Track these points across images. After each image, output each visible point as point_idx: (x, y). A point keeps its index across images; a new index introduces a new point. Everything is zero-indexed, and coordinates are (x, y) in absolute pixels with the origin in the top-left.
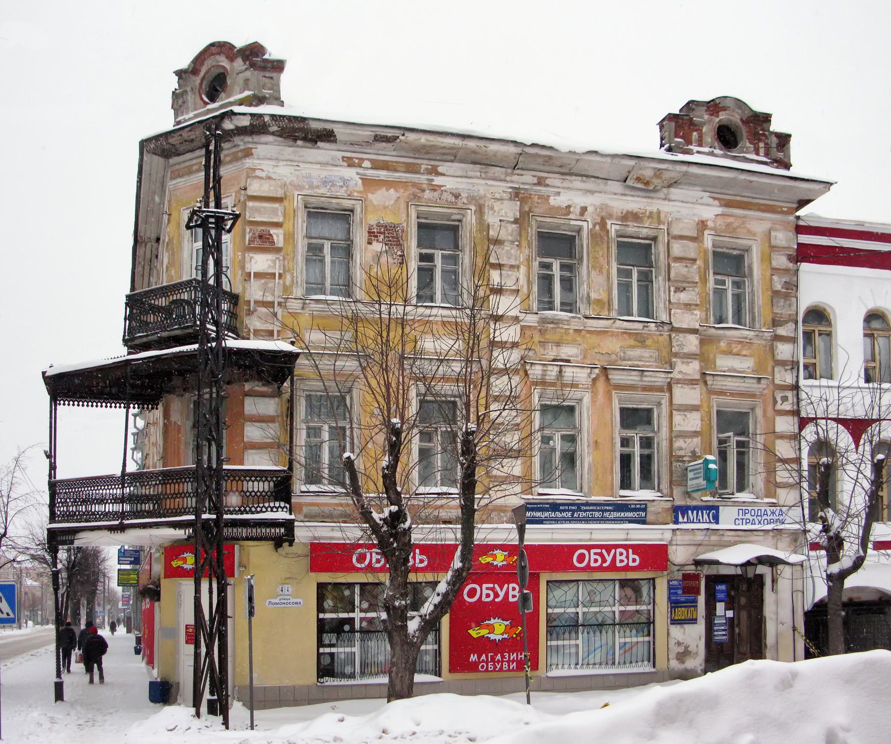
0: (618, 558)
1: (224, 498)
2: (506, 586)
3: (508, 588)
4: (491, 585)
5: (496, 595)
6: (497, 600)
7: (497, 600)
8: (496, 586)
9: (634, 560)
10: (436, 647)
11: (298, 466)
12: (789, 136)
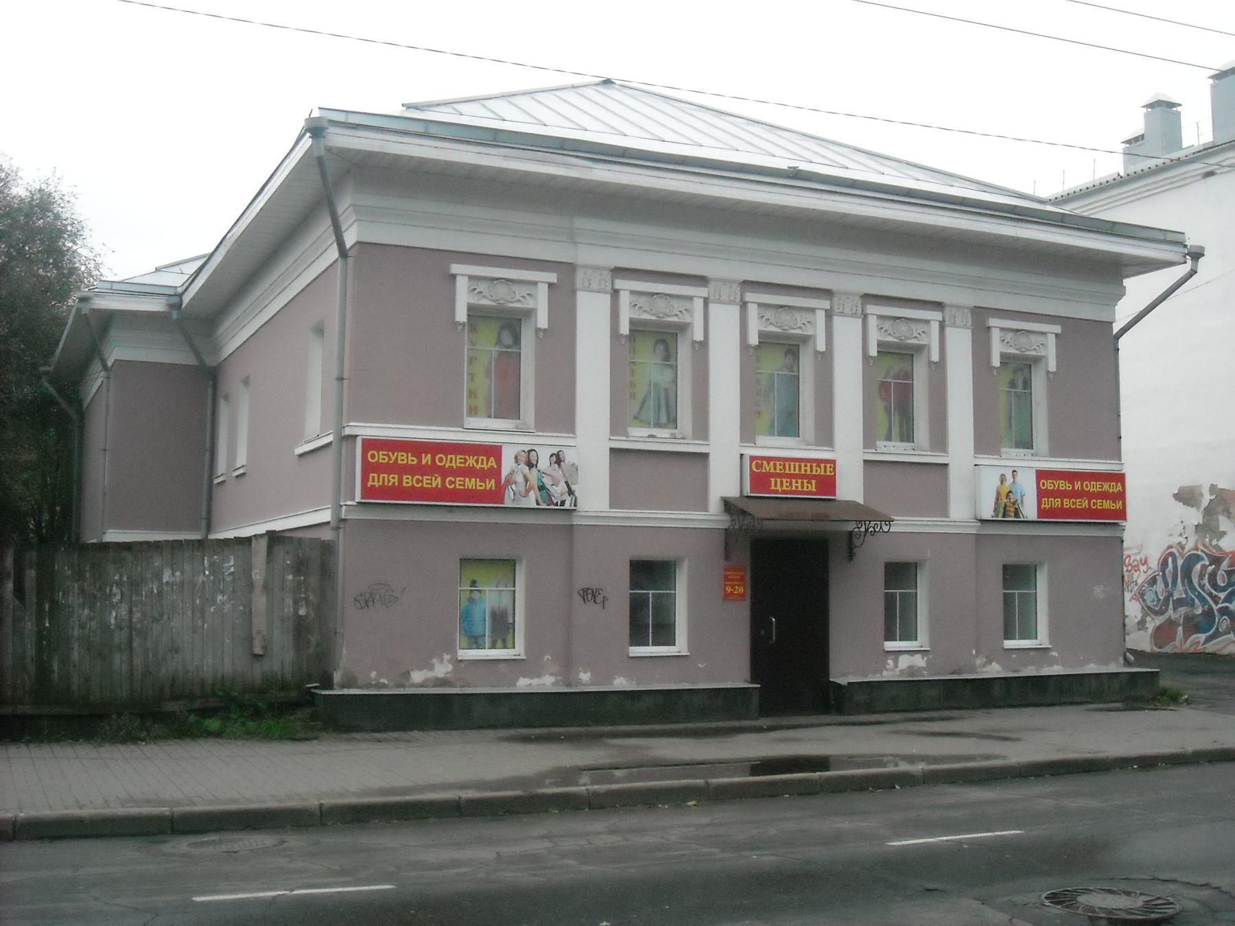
0: (1061, 485)
1: (187, 299)
2: (396, 453)
3: (397, 455)
4: (386, 453)
5: (390, 459)
6: (391, 462)
7: (391, 462)
8: (390, 453)
9: (1069, 487)
10: (1035, 591)
11: (99, 367)
12: (709, 453)
